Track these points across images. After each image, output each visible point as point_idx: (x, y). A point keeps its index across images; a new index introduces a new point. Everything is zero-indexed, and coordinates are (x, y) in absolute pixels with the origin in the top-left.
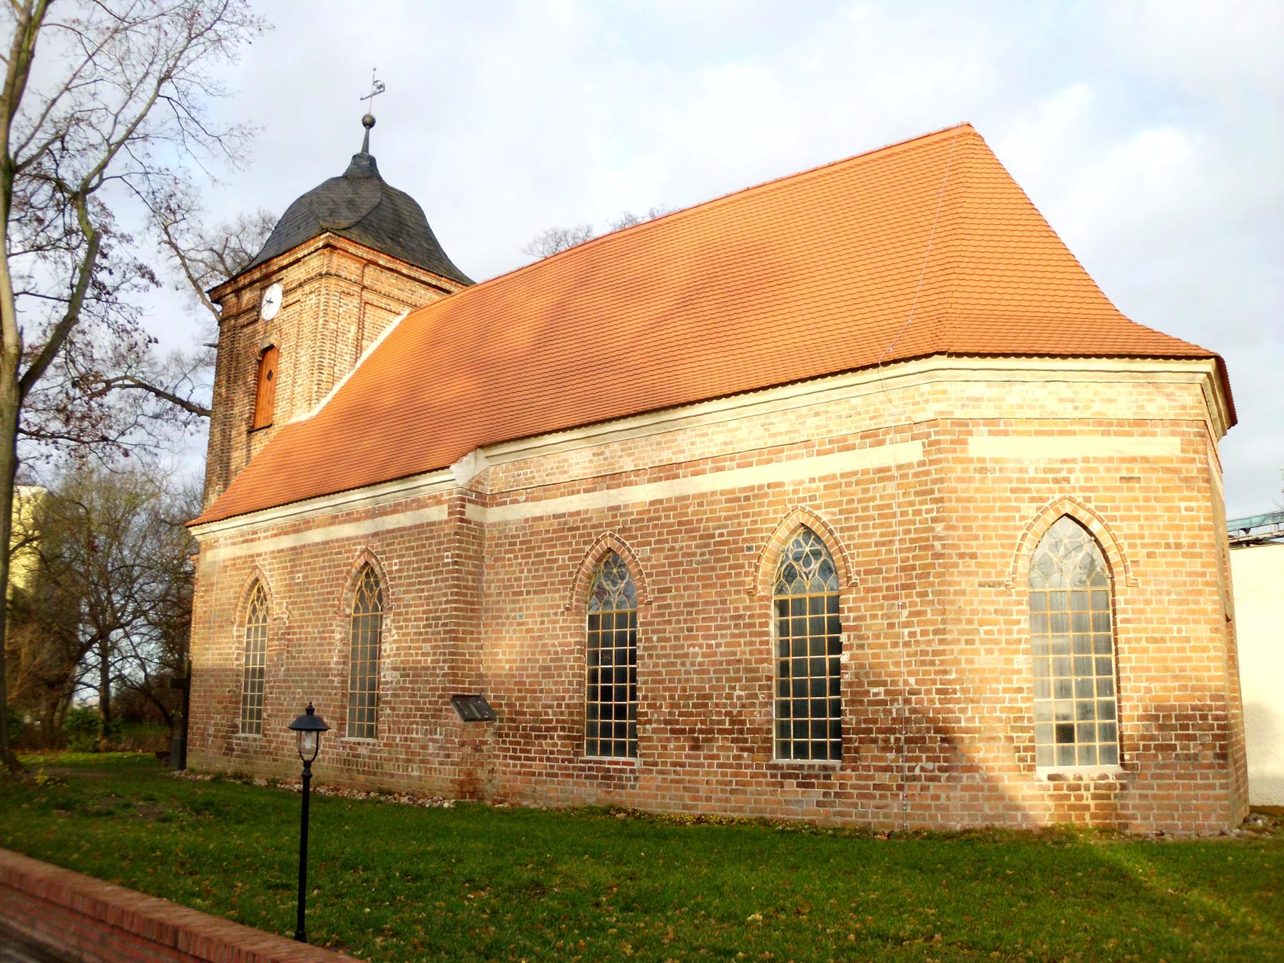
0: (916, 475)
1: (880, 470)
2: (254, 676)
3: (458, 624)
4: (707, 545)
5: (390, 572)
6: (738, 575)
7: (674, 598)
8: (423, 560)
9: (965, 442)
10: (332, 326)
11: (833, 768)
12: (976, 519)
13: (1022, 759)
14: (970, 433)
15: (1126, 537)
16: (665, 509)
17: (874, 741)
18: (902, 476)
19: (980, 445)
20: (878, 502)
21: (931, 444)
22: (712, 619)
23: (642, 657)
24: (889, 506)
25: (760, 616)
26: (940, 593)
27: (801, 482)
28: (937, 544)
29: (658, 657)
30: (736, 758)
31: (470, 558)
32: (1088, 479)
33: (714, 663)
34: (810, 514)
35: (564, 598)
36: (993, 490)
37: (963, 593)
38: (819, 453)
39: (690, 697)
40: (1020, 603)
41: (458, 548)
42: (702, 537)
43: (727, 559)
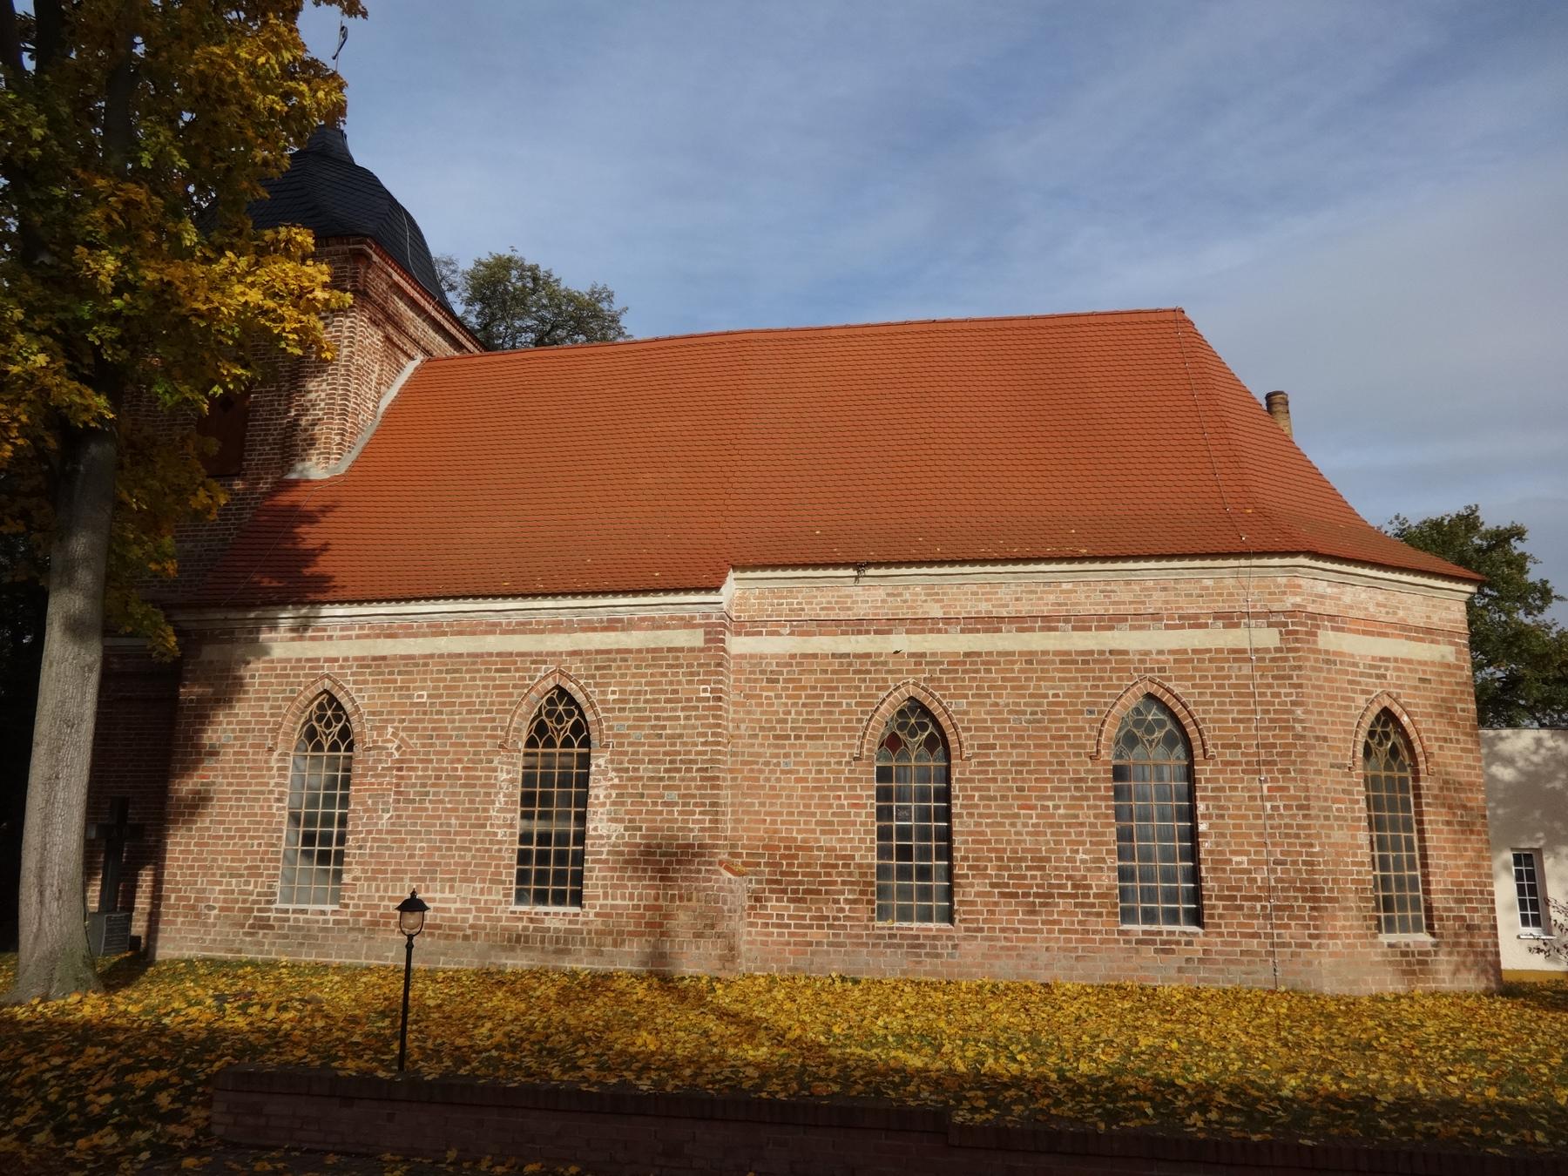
0: (1273, 660)
9: (1315, 634)
14: (1318, 627)
17: (1240, 908)
21: (1289, 633)
29: (980, 816)
33: (1051, 825)
34: (1160, 685)
38: (1168, 627)
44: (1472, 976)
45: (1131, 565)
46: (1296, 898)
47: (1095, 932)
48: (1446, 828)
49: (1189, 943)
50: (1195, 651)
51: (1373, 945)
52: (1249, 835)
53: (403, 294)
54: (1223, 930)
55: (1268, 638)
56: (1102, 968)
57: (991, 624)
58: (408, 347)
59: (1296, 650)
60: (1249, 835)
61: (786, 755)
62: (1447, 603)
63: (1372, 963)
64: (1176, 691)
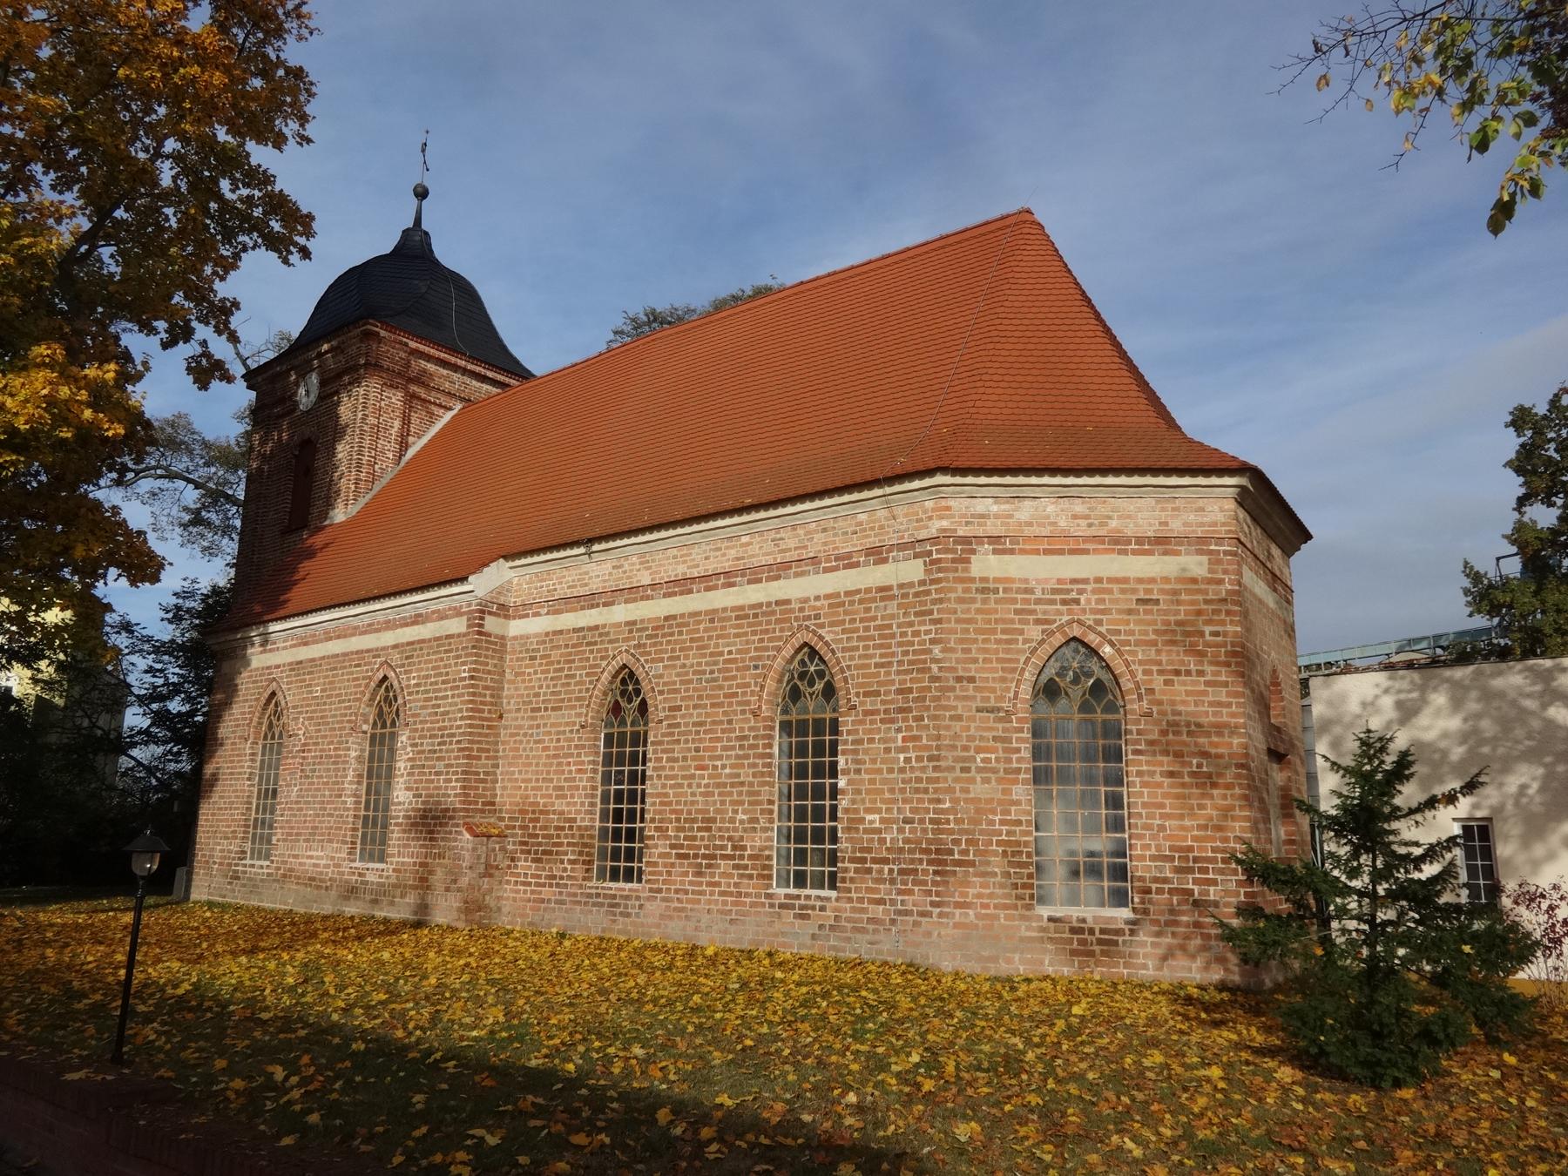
0: (917, 595)
1: (881, 589)
2: (266, 797)
3: (470, 742)
4: (716, 663)
5: (408, 686)
6: (744, 694)
7: (683, 716)
8: (440, 674)
9: (968, 561)
10: (372, 420)
11: (828, 899)
12: (975, 641)
13: (1018, 897)
14: (974, 552)
15: (1141, 663)
16: (678, 625)
17: (869, 871)
18: (905, 596)
19: (985, 564)
20: (878, 622)
21: (933, 562)
22: (719, 739)
23: (651, 777)
24: (890, 626)
25: (764, 737)
26: (935, 718)
27: (806, 600)
28: (934, 667)
29: (667, 777)
30: (736, 885)
31: (489, 672)
32: (1099, 601)
33: (718, 785)
34: (814, 632)
35: (579, 715)
36: (996, 611)
37: (959, 718)
38: (826, 570)
39: (694, 820)
40: (1021, 730)
41: (475, 662)
42: (712, 654)
43: (734, 678)
44: (1199, 962)
45: (790, 509)
46: (921, 861)
47: (747, 895)
48: (1167, 781)
49: (822, 909)
50: (847, 593)
51: (1023, 918)
52: (882, 791)
53: (429, 358)
54: (854, 895)
55: (912, 570)
56: (745, 935)
57: (682, 585)
58: (443, 400)
59: (938, 581)
60: (882, 791)
61: (538, 726)
62: (1201, 503)
63: (1022, 939)
64: (827, 638)
